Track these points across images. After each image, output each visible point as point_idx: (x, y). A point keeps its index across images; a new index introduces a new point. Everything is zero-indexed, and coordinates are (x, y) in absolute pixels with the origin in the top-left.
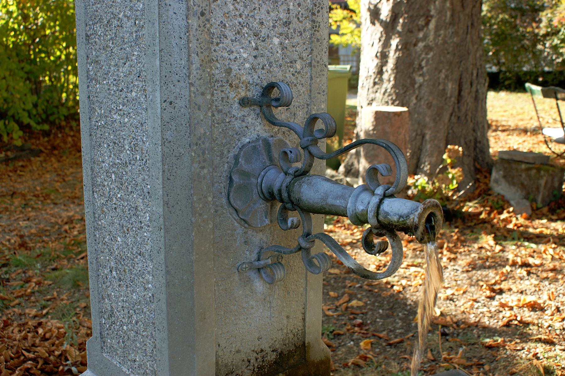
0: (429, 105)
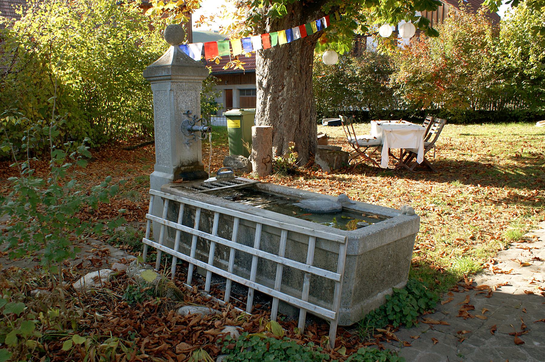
0: (285, 125)
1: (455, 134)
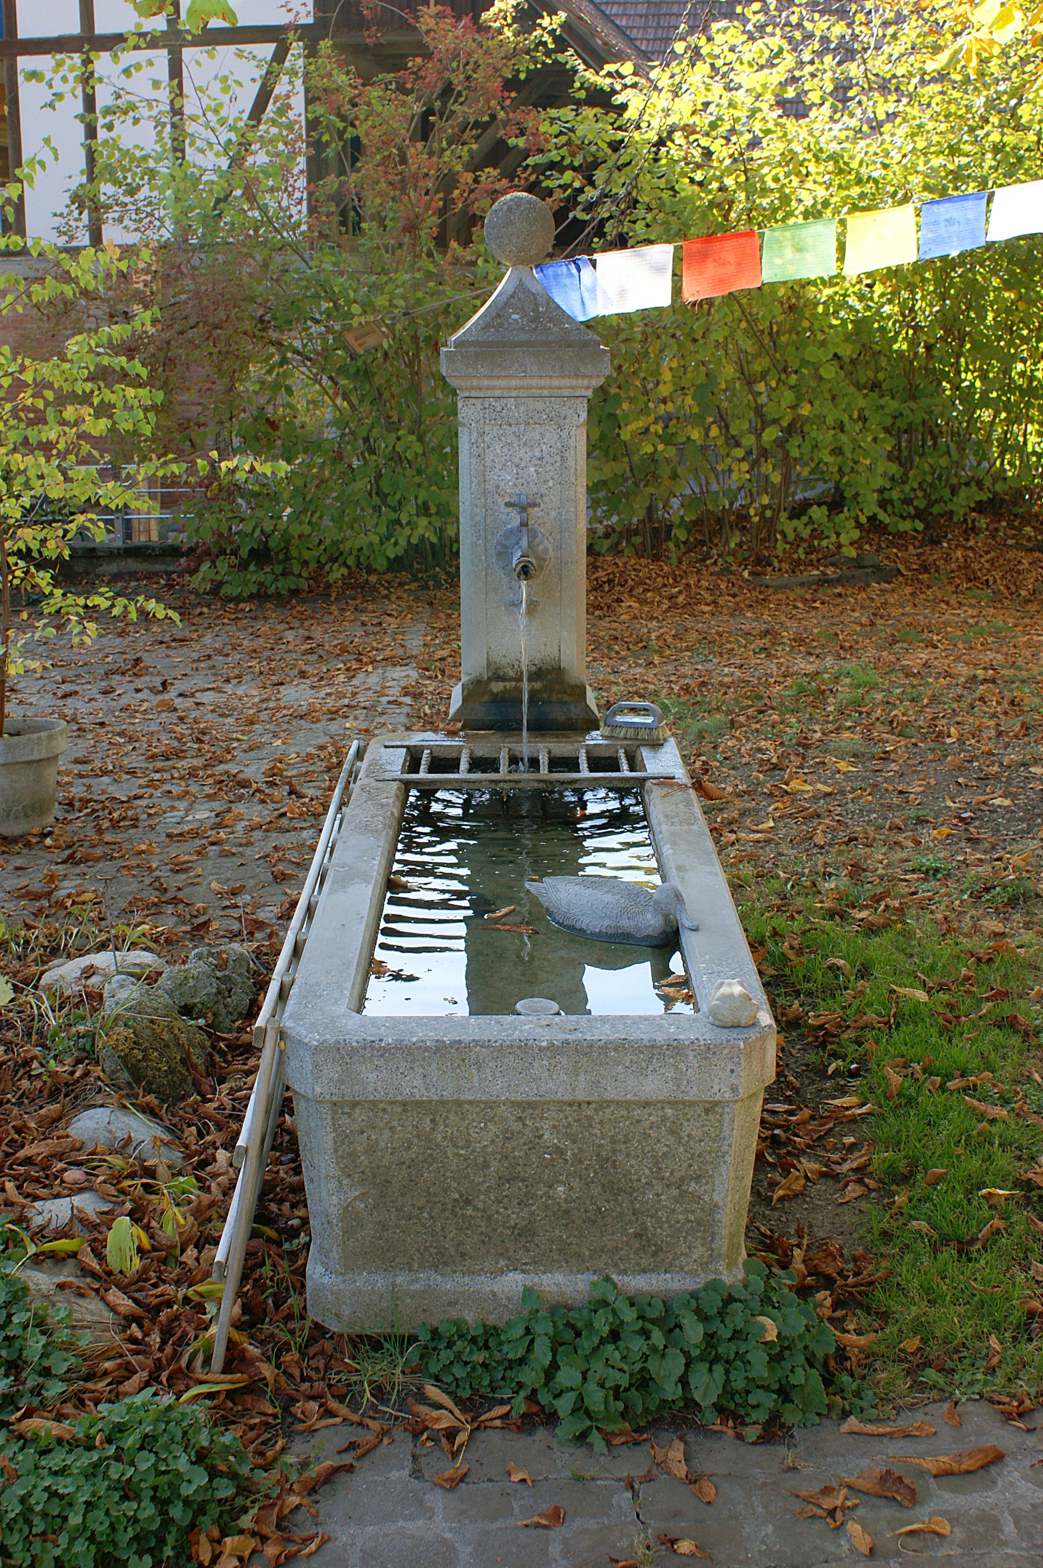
1: (361, 130)
